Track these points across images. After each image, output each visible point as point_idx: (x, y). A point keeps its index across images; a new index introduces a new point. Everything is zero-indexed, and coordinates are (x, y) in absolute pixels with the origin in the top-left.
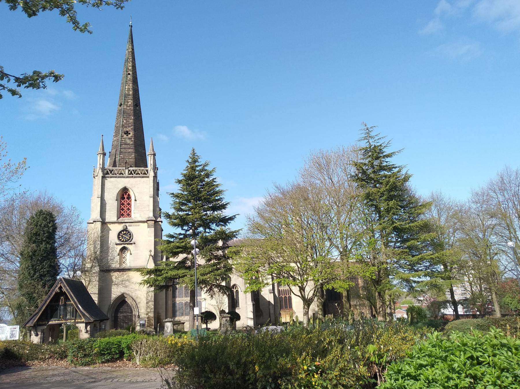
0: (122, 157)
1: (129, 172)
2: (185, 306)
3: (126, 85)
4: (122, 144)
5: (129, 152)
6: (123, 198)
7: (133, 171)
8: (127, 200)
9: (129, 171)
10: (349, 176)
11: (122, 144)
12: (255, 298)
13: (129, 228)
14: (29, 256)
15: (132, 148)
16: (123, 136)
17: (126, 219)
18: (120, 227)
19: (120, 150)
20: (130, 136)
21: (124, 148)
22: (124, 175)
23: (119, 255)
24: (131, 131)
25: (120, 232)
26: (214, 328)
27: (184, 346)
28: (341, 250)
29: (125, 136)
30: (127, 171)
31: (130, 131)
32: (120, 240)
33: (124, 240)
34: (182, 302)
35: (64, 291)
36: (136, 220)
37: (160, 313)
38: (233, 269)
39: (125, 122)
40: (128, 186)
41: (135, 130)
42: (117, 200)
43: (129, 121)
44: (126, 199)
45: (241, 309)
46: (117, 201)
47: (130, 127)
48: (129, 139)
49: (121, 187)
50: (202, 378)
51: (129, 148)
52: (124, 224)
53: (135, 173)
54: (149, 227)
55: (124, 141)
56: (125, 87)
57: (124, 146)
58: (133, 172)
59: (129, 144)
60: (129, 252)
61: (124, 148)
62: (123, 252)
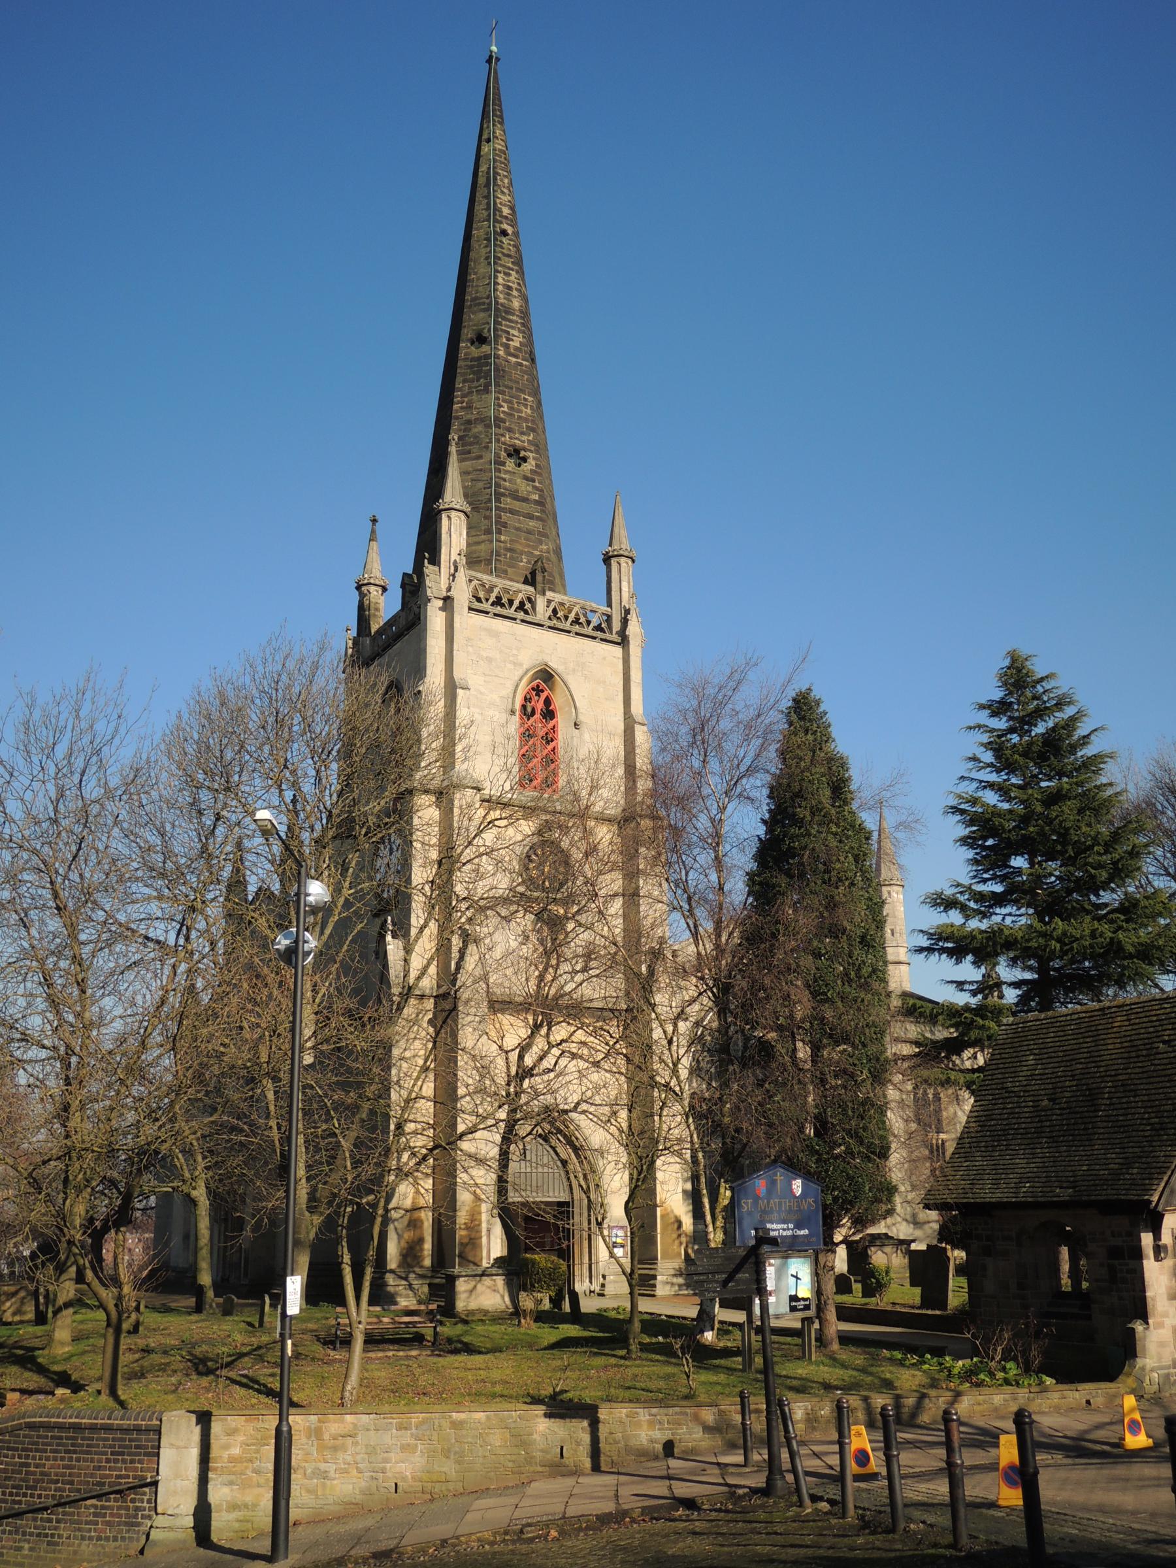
3: (497, 271)
4: (503, 495)
5: (529, 532)
9: (549, 602)
10: (427, 888)
11: (503, 495)
21: (512, 512)
24: (531, 451)
26: (830, 718)
27: (32, 1190)
29: (510, 464)
31: (525, 449)
38: (414, 844)
39: (506, 409)
40: (555, 664)
41: (463, 301)
43: (520, 411)
47: (522, 433)
50: (1161, 824)
56: (496, 277)
59: (525, 500)
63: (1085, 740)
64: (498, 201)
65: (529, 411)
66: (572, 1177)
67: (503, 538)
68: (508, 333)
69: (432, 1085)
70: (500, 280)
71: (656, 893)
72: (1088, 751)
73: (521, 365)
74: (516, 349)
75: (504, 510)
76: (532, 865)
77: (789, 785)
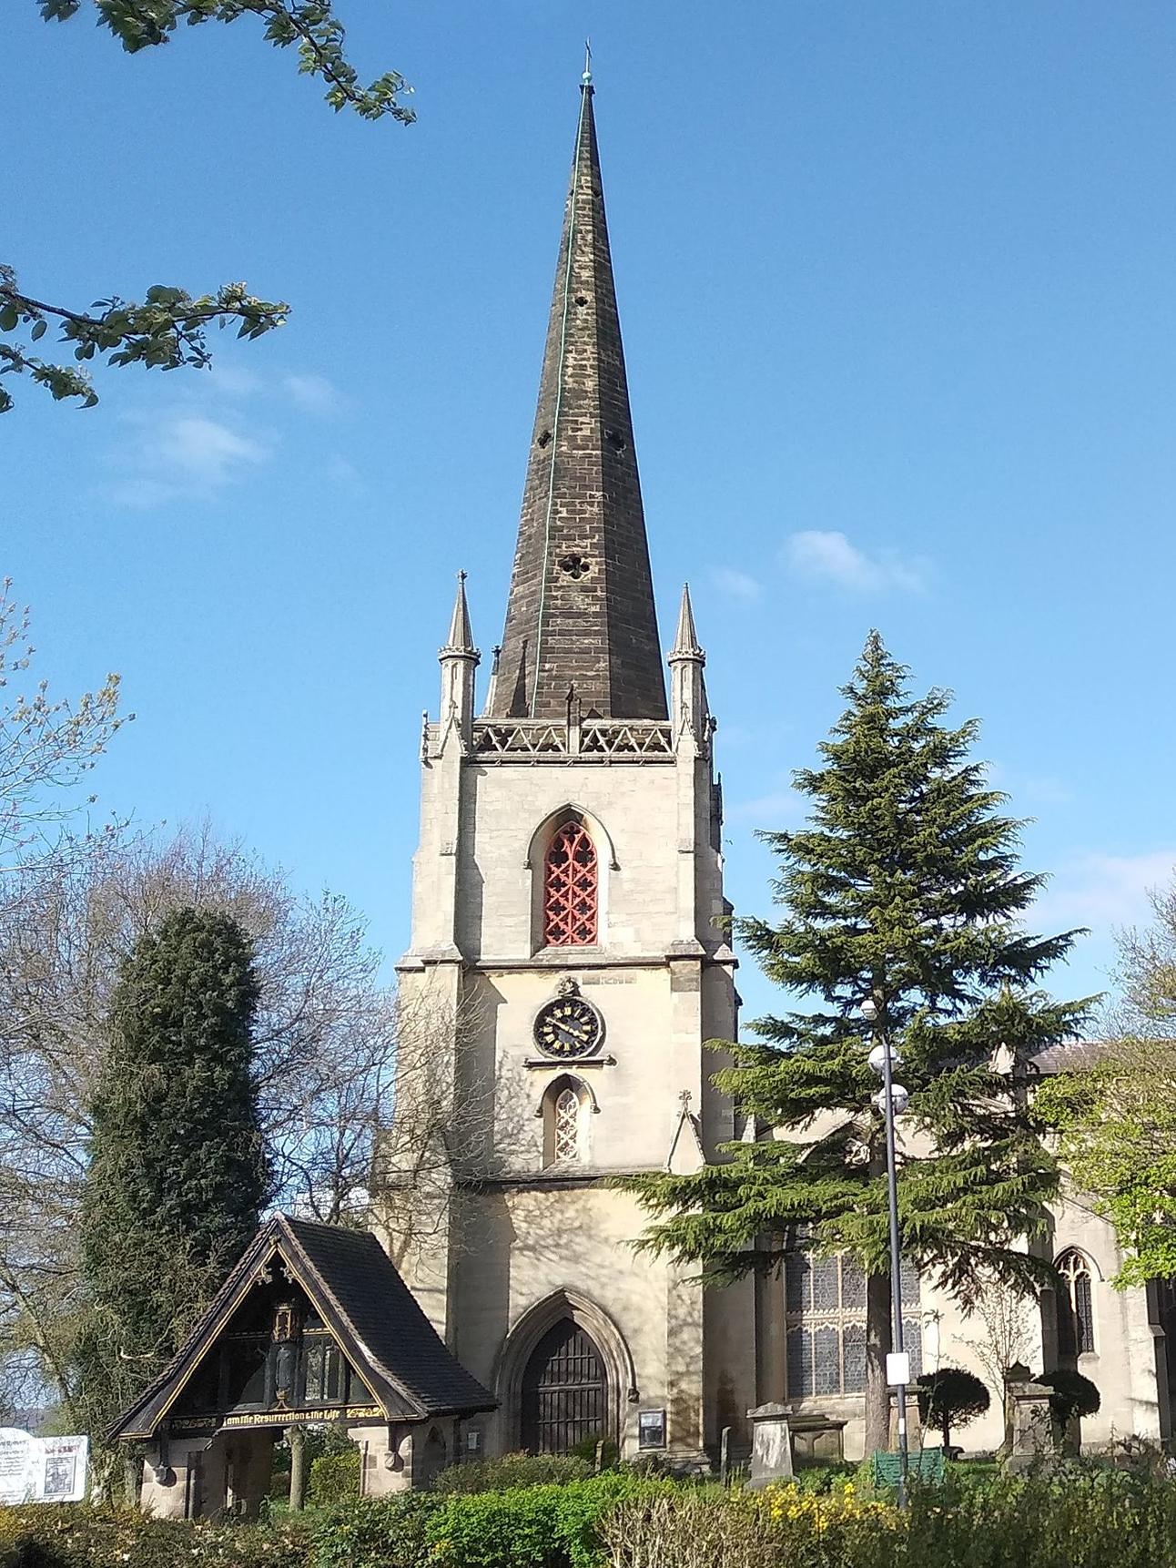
1: (586, 740)
5: (585, 651)
6: (558, 856)
7: (604, 733)
9: (585, 733)
11: (553, 616)
13: (589, 994)
15: (597, 633)
16: (556, 580)
17: (574, 953)
18: (545, 989)
19: (545, 642)
20: (586, 577)
22: (563, 754)
25: (548, 1010)
29: (565, 578)
30: (575, 734)
32: (548, 1046)
33: (562, 1047)
35: (294, 1280)
36: (620, 955)
37: (732, 1381)
40: (581, 802)
42: (529, 866)
43: (584, 512)
44: (570, 860)
49: (548, 804)
51: (586, 634)
52: (564, 974)
54: (676, 986)
56: (566, 359)
58: (602, 741)
60: (588, 1102)
63: (985, 802)
64: (576, 265)
65: (596, 509)
66: (266, 1246)
67: (547, 666)
68: (576, 422)
69: (510, 1315)
70: (571, 362)
71: (1073, 1148)
72: (986, 816)
73: (590, 456)
74: (585, 438)
75: (552, 634)
76: (550, 1038)
77: (1005, 937)
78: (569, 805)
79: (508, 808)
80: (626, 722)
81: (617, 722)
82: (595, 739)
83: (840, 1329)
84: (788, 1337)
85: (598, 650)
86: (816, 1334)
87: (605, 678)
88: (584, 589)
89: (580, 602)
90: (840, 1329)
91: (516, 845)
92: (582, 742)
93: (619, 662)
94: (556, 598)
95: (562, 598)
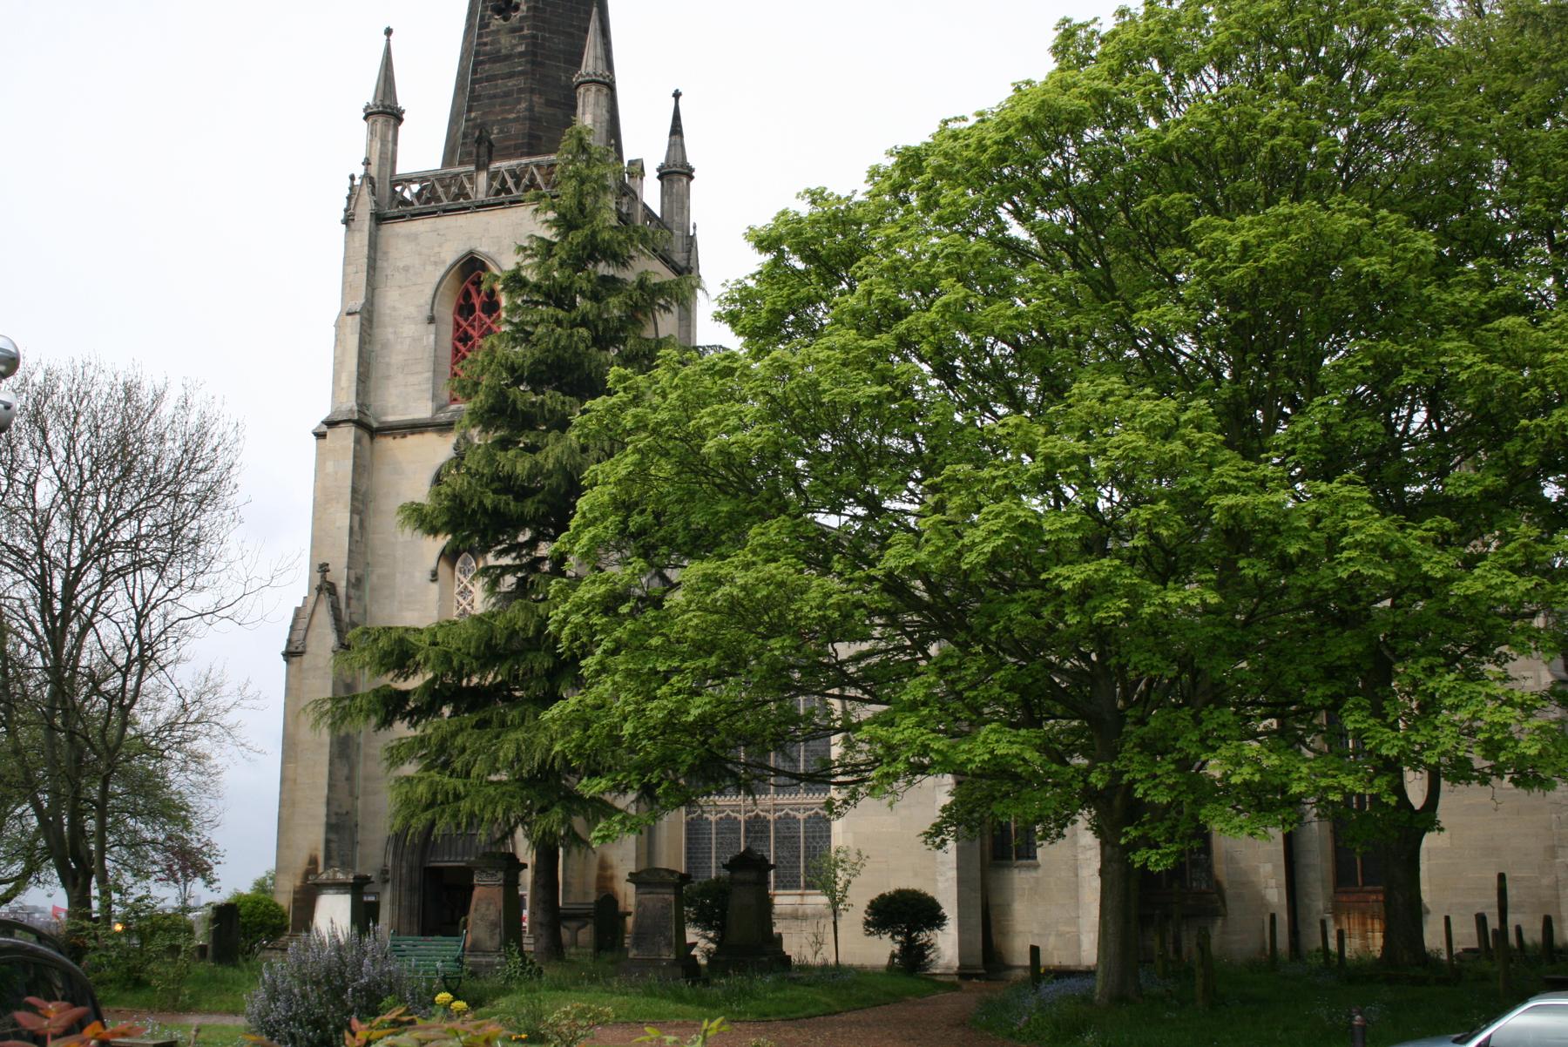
0: (475, 118)
2: (746, 837)
5: (507, 94)
6: (464, 308)
7: (512, 173)
8: (482, 315)
9: (493, 176)
11: (482, 63)
12: (588, 116)
14: (1483, 412)
15: (521, 73)
16: (487, 25)
19: (472, 91)
20: (516, 16)
21: (488, 79)
23: (434, 576)
28: (1457, 589)
30: (482, 178)
34: (733, 815)
37: (611, 867)
40: (484, 248)
42: (432, 320)
44: (478, 312)
45: (1039, 874)
46: (432, 327)
48: (513, 30)
49: (451, 254)
51: (511, 75)
53: (517, 185)
55: (488, 48)
57: (487, 67)
58: (510, 183)
61: (488, 79)
62: (459, 565)
78: (471, 252)
79: (1319, 416)
80: (534, 159)
81: (525, 161)
82: (504, 181)
83: (741, 818)
84: (688, 823)
85: (520, 91)
86: (717, 823)
87: (525, 118)
88: (513, 30)
89: (505, 41)
90: (741, 818)
91: (422, 301)
92: (490, 186)
93: (542, 101)
94: (485, 44)
95: (492, 43)
